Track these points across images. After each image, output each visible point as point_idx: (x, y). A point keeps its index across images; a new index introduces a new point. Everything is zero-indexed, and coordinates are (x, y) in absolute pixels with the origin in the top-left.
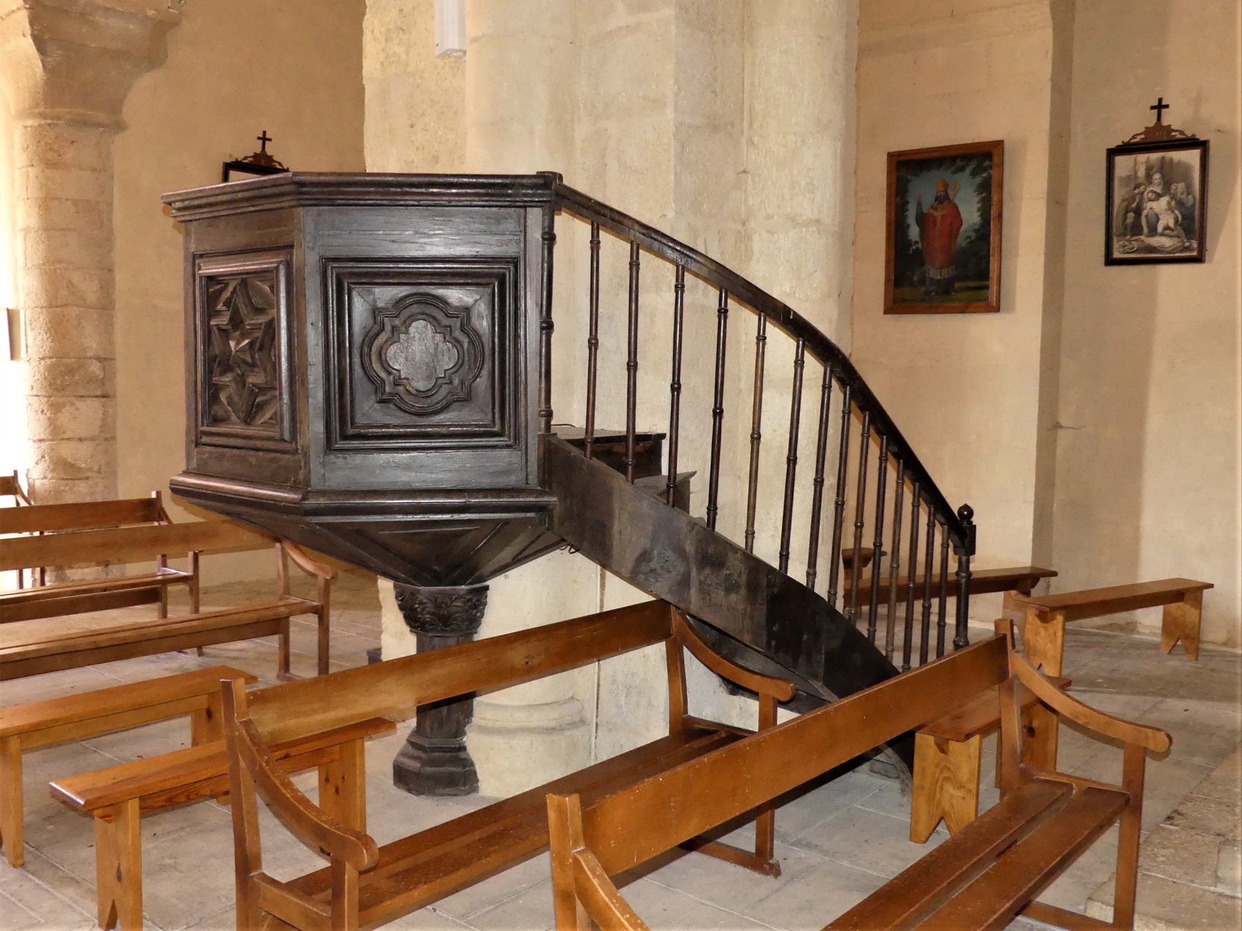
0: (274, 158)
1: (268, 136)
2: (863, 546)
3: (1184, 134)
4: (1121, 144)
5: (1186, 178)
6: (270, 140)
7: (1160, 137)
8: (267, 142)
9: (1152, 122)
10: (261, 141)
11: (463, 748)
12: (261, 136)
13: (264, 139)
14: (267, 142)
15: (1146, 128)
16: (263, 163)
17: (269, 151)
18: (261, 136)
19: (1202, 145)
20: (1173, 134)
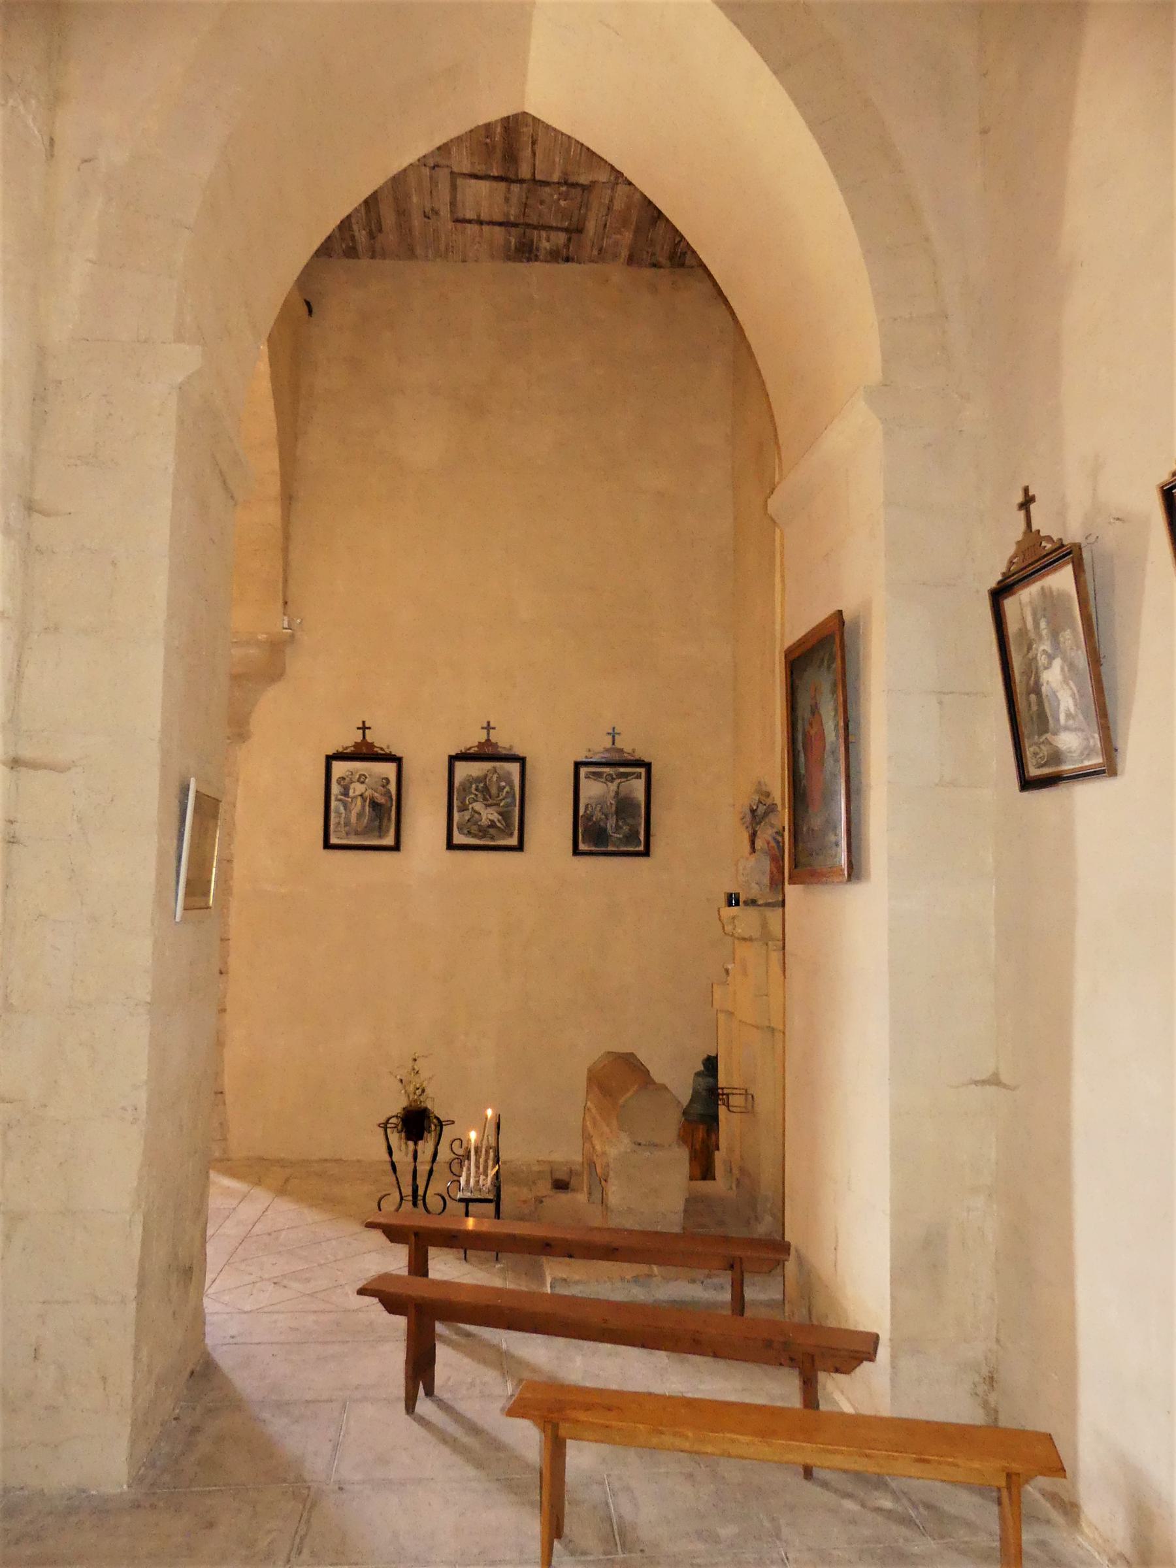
0: (375, 744)
1: (367, 725)
2: (677, 1230)
3: (383, 750)
4: (336, 752)
5: (510, 783)
6: (369, 728)
7: (489, 750)
8: (367, 731)
9: (359, 739)
10: (361, 731)
11: (136, 1341)
12: (361, 726)
13: (488, 727)
14: (367, 731)
15: (479, 743)
16: (364, 750)
17: (369, 739)
18: (361, 726)
19: (522, 760)
20: (376, 749)
